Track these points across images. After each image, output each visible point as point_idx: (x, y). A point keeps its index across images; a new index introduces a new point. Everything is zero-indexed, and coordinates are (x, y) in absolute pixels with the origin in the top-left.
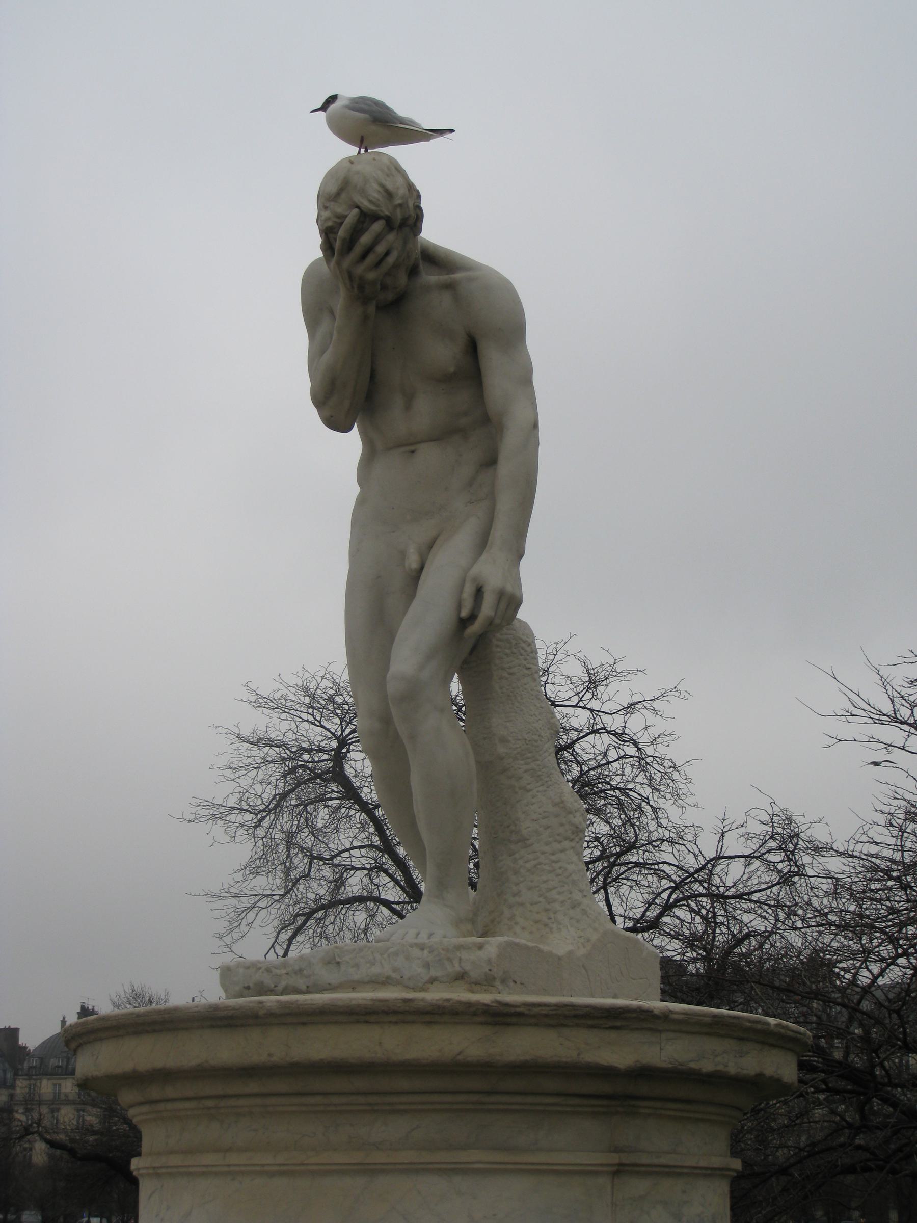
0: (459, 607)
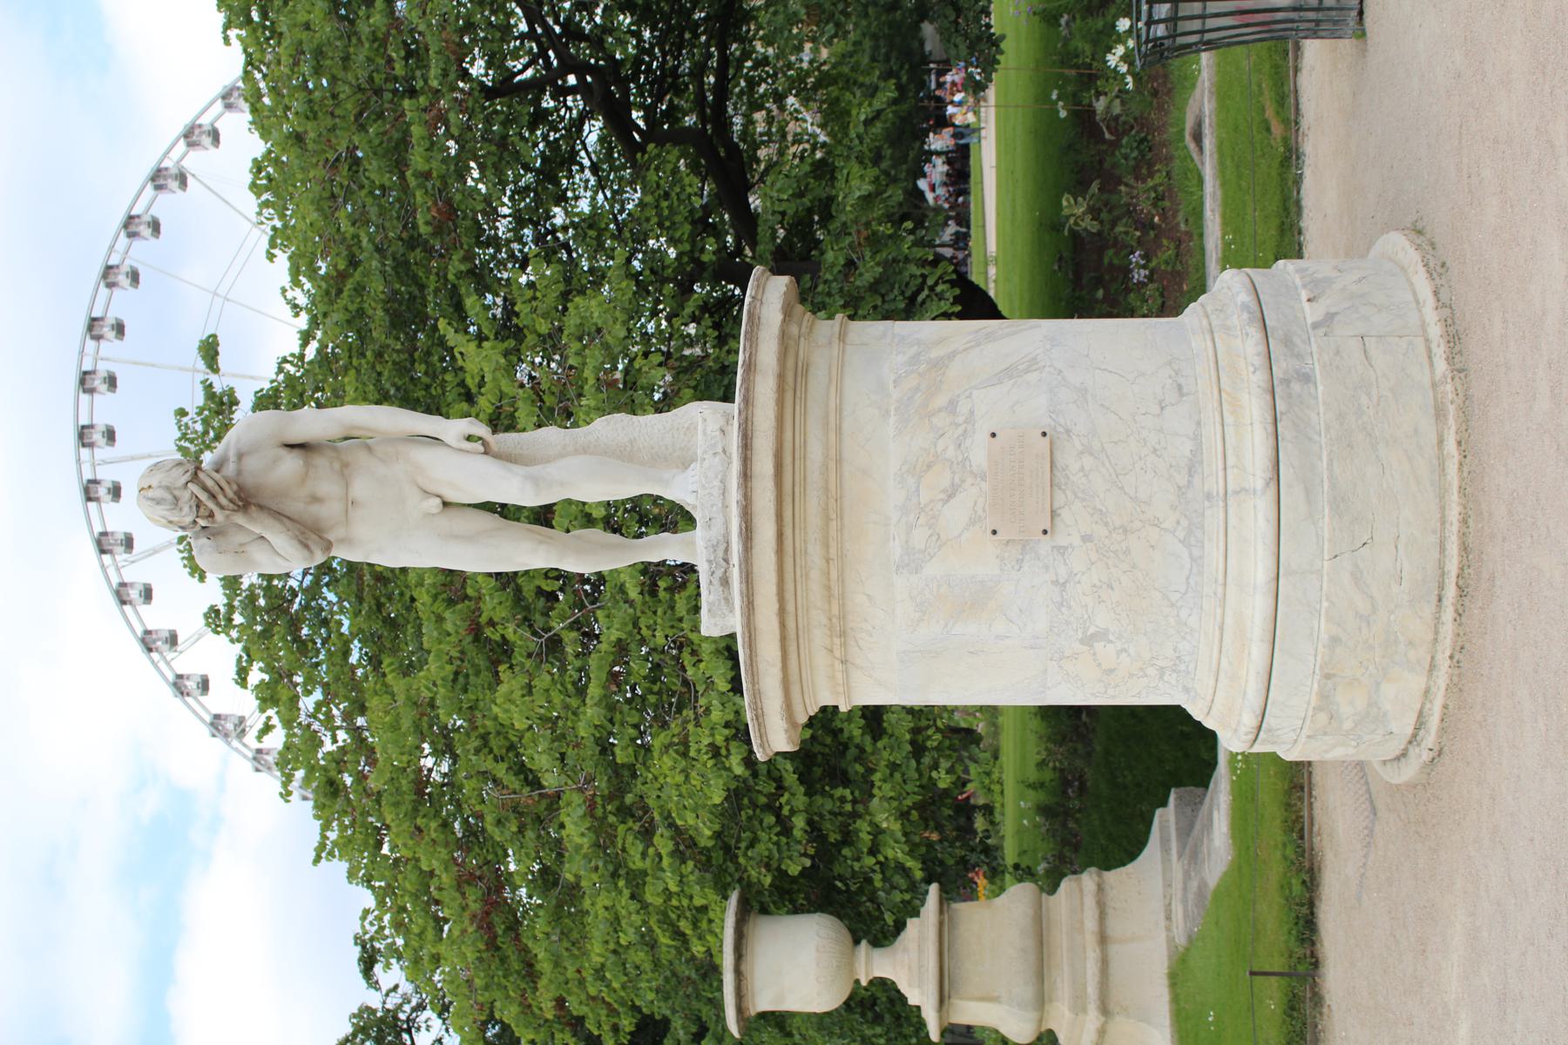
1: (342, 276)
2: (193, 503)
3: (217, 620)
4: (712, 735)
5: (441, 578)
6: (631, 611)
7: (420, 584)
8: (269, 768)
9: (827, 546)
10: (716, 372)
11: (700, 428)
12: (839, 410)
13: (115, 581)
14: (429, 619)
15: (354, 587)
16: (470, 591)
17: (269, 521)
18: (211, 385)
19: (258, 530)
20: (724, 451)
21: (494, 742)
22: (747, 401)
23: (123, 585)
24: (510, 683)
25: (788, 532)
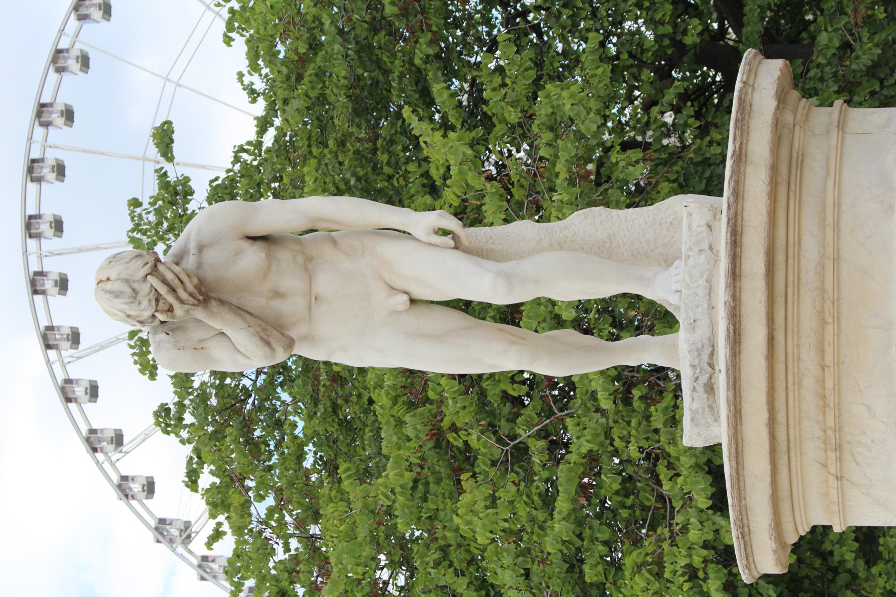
0: (447, 248)
1: (303, 61)
2: (152, 297)
3: (167, 419)
4: (690, 556)
5: (402, 380)
6: (603, 420)
7: (379, 386)
8: (215, 577)
9: (822, 352)
10: (697, 164)
11: (685, 222)
12: (838, 205)
13: (61, 377)
14: (388, 423)
15: (310, 388)
16: (431, 394)
17: (230, 316)
18: (165, 174)
19: (217, 325)
20: (711, 248)
21: (457, 556)
22: (737, 194)
23: (68, 381)
24: (473, 494)
25: (780, 336)
